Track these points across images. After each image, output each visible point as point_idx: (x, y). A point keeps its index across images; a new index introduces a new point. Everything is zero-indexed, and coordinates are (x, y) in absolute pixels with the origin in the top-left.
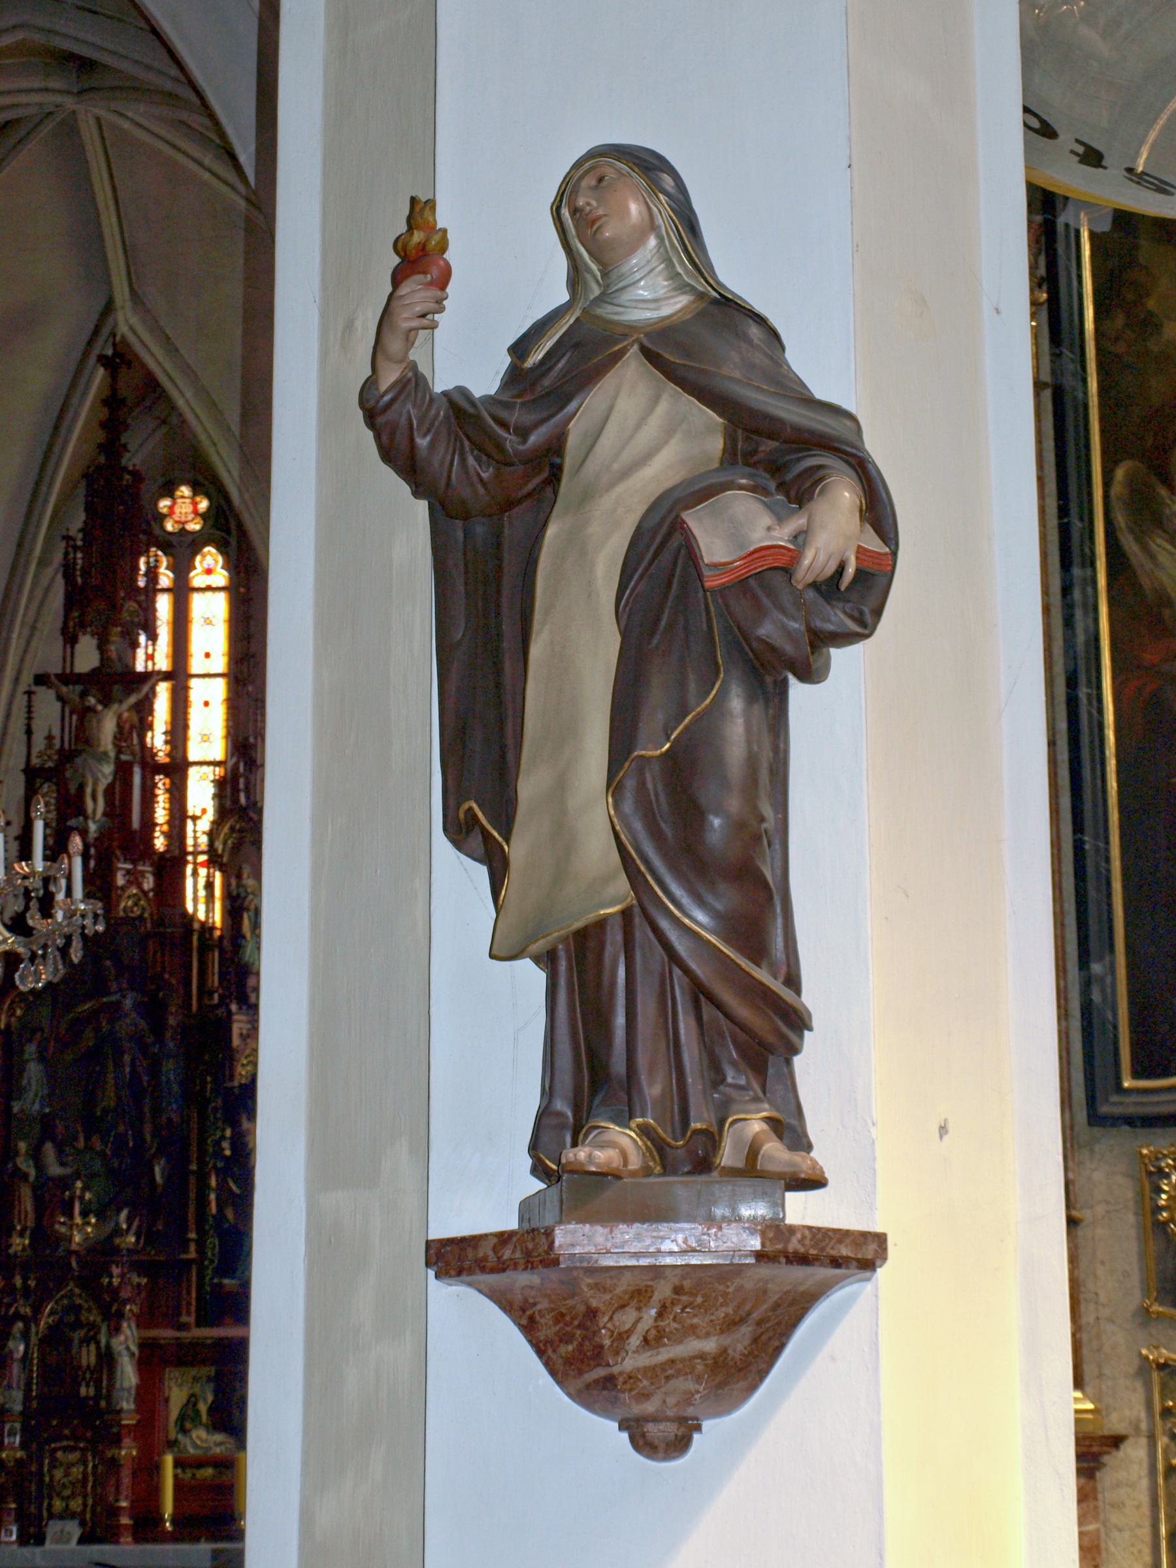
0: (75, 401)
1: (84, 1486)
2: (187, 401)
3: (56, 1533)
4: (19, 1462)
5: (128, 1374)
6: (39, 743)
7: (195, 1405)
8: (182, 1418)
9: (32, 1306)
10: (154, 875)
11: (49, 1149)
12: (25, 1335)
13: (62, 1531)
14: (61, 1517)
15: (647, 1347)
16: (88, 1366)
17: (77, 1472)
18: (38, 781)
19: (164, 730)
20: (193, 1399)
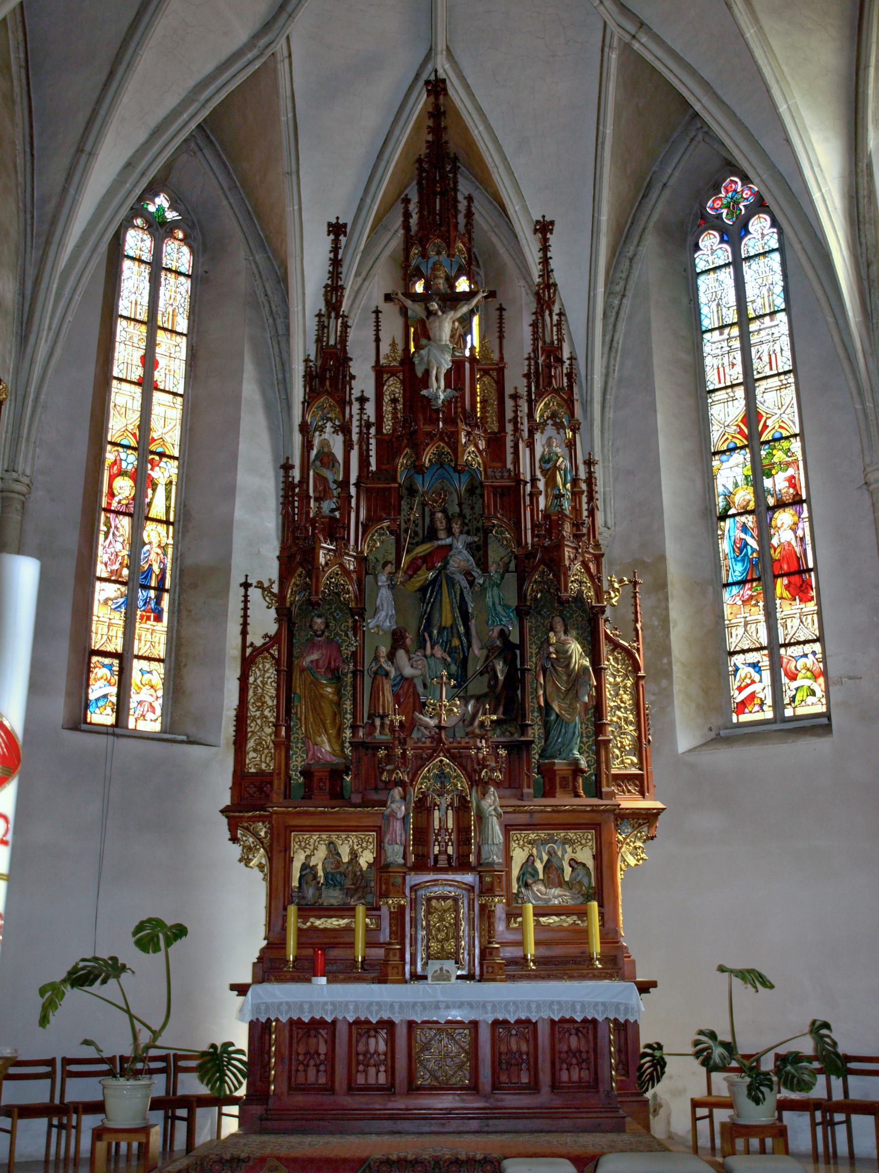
0: (396, 133)
2: (479, 132)
3: (436, 971)
11: (401, 654)
13: (441, 969)
18: (385, 377)
19: (538, 261)
20: (532, 858)
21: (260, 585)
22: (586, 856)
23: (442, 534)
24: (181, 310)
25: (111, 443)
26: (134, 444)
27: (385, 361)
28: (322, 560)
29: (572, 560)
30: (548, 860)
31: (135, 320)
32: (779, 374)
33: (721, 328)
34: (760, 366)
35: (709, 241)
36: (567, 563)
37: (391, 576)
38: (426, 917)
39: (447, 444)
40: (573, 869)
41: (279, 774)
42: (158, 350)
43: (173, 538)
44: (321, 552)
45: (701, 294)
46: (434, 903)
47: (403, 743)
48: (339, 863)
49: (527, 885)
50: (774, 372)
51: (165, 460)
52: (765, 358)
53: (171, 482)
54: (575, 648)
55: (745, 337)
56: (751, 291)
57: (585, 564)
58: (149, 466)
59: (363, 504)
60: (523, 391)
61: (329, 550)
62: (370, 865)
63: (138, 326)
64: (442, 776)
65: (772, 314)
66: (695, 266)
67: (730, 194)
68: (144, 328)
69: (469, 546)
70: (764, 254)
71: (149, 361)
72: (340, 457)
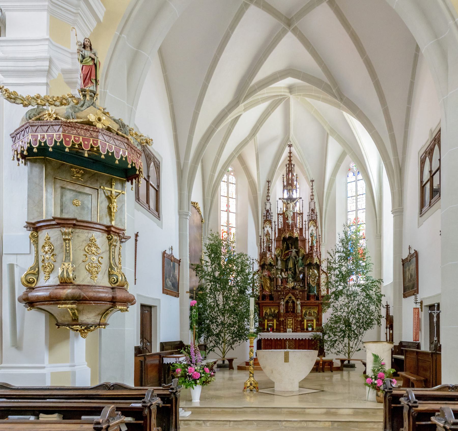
6: (279, 210)
11: (283, 273)
14: (289, 328)
15: (24, 297)
17: (291, 322)
21: (256, 260)
22: (316, 311)
23: (290, 248)
26: (226, 225)
28: (268, 256)
29: (315, 256)
34: (359, 207)
37: (281, 258)
47: (283, 291)
48: (271, 312)
49: (305, 316)
55: (357, 199)
57: (318, 257)
59: (275, 242)
60: (307, 220)
62: (277, 312)
64: (290, 297)
68: (226, 198)
69: (296, 251)
71: (228, 206)
72: (271, 233)
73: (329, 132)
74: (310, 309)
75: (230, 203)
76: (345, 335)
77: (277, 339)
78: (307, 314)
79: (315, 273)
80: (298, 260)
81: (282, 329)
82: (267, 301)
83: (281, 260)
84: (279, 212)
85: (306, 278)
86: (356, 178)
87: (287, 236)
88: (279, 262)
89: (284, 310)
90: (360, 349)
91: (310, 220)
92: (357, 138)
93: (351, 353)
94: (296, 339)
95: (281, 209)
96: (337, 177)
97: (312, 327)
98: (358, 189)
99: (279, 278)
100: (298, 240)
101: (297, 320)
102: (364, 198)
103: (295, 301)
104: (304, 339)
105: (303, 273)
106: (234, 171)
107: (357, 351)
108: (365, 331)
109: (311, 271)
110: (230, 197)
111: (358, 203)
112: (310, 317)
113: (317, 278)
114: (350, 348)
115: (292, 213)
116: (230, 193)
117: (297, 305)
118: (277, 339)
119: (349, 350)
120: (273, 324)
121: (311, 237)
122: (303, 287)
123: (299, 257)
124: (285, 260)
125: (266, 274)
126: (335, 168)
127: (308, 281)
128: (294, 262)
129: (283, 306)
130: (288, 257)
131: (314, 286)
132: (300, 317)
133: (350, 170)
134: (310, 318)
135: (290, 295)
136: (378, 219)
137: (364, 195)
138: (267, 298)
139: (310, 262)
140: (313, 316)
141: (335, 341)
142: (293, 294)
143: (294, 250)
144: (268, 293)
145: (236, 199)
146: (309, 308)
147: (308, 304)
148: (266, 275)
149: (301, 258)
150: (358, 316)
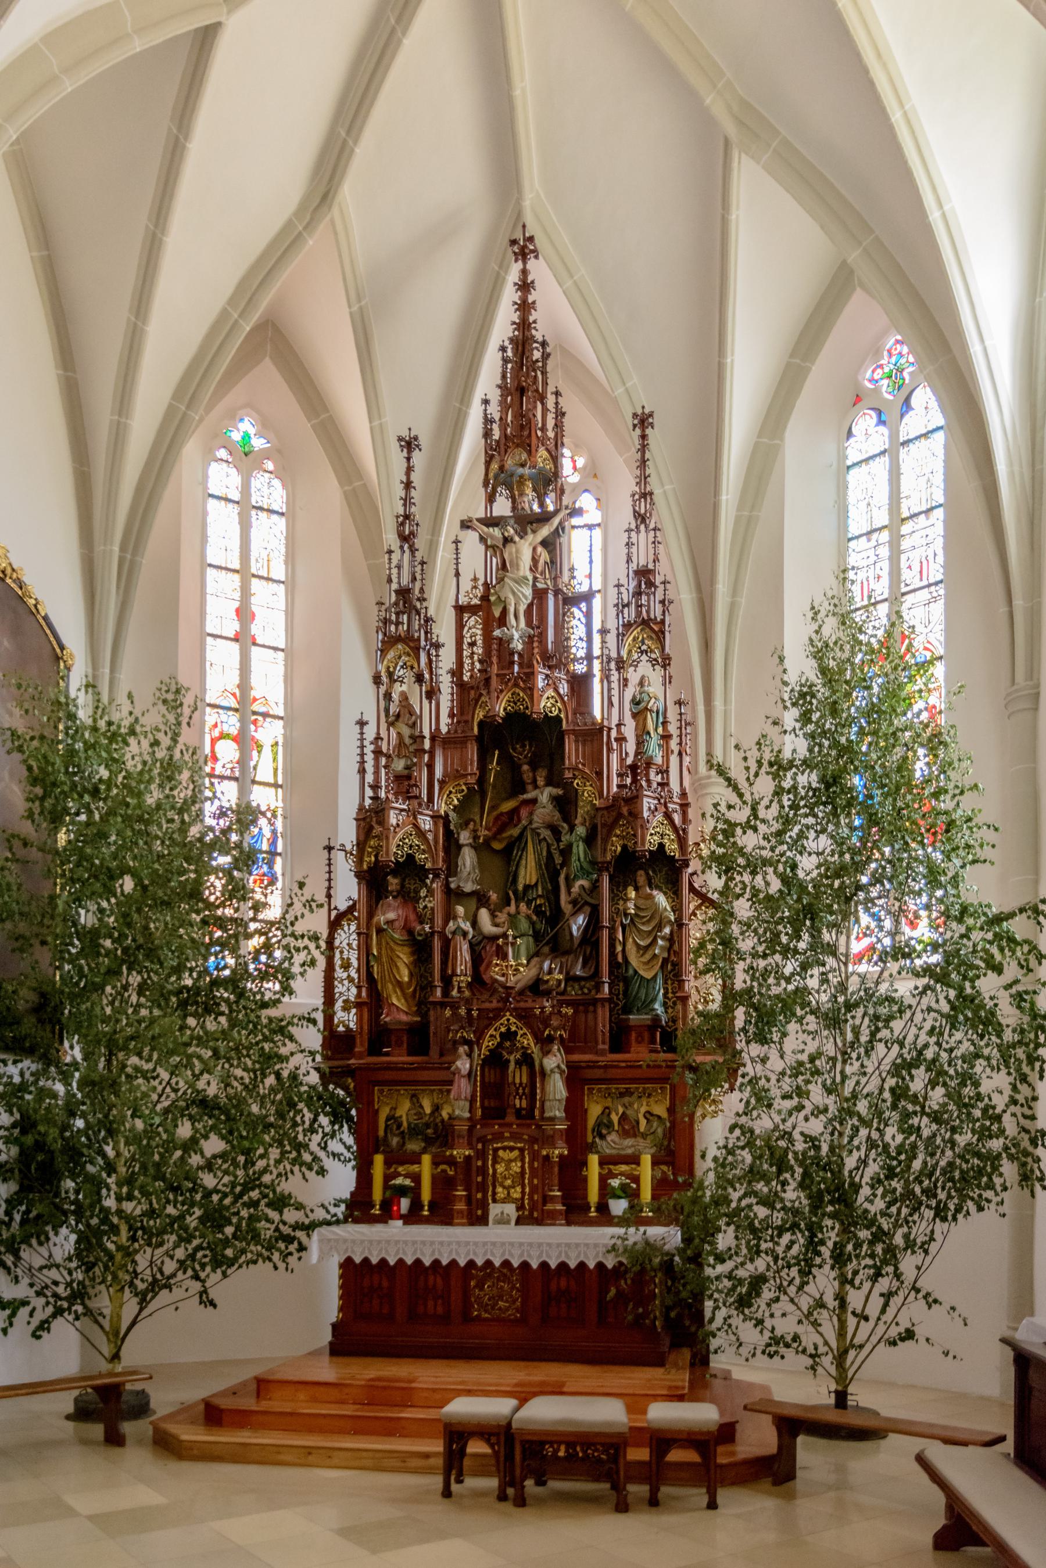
1: (523, 1178)
4: (468, 1158)
5: (557, 1089)
6: (466, 585)
7: (609, 1114)
8: (599, 1124)
9: (474, 1032)
10: (568, 682)
12: (469, 1055)
14: (504, 1201)
16: (521, 1084)
17: (516, 1167)
22: (661, 1110)
24: (276, 554)
25: (209, 705)
27: (467, 599)
28: (393, 821)
30: (624, 1113)
31: (227, 569)
32: (929, 586)
33: (869, 533)
34: (910, 577)
35: (865, 423)
36: (646, 814)
38: (493, 1166)
39: (523, 690)
40: (648, 1120)
41: (361, 1033)
42: (253, 600)
43: (283, 801)
44: (392, 813)
45: (850, 493)
46: (501, 1153)
48: (420, 1115)
49: (602, 1137)
50: (925, 583)
51: (268, 720)
52: (916, 568)
53: (277, 743)
54: (661, 900)
56: (907, 484)
57: (668, 816)
58: (253, 727)
60: (612, 624)
61: (402, 810)
63: (230, 575)
64: (509, 1036)
65: (928, 511)
66: (846, 457)
67: (893, 360)
68: (236, 577)
69: (555, 800)
70: (925, 435)
71: (244, 613)
73: (730, 129)
74: (626, 1100)
75: (253, 600)
76: (813, 1245)
77: (418, 1262)
78: (609, 1125)
79: (656, 905)
80: (570, 846)
81: (461, 1206)
82: (400, 1058)
83: (476, 847)
84: (463, 600)
85: (605, 933)
86: (894, 435)
87: (500, 708)
88: (468, 858)
89: (472, 1101)
90: (909, 1335)
91: (628, 626)
92: (896, 117)
93: (852, 1353)
94: (525, 1265)
95: (475, 579)
96: (788, 434)
97: (632, 1194)
98: (905, 490)
99: (459, 938)
100: (561, 736)
101: (547, 1158)
102: (939, 529)
103: (535, 1050)
104: (572, 1265)
105: (587, 909)
106: (279, 451)
107: (894, 1343)
108: (939, 1227)
109: (632, 894)
110: (254, 571)
111: (903, 557)
112: (629, 1142)
113: (667, 930)
114: (851, 1321)
115: (528, 592)
116: (254, 555)
117: (543, 1074)
118: (366, 1260)
119: (841, 1333)
120: (417, 1178)
121: (635, 716)
122: (590, 984)
123: (572, 829)
124: (497, 846)
125: (391, 915)
126: (781, 383)
127: (619, 948)
128: (550, 855)
129: (464, 1082)
130: (515, 832)
131: (648, 975)
132: (560, 1143)
133: (858, 399)
134: (628, 1146)
135: (509, 1021)
136: (1018, 602)
137: (939, 513)
138: (399, 1044)
139: (624, 847)
140: (644, 1136)
141: (757, 1282)
142: (525, 1016)
143: (545, 795)
144: (404, 1018)
145: (290, 584)
146: (622, 1095)
147: (612, 1073)
148: (389, 922)
149: (581, 830)
150: (899, 1138)
